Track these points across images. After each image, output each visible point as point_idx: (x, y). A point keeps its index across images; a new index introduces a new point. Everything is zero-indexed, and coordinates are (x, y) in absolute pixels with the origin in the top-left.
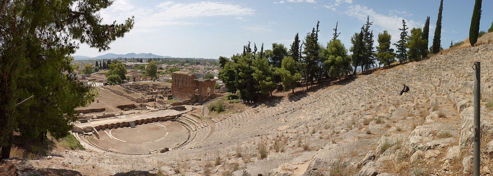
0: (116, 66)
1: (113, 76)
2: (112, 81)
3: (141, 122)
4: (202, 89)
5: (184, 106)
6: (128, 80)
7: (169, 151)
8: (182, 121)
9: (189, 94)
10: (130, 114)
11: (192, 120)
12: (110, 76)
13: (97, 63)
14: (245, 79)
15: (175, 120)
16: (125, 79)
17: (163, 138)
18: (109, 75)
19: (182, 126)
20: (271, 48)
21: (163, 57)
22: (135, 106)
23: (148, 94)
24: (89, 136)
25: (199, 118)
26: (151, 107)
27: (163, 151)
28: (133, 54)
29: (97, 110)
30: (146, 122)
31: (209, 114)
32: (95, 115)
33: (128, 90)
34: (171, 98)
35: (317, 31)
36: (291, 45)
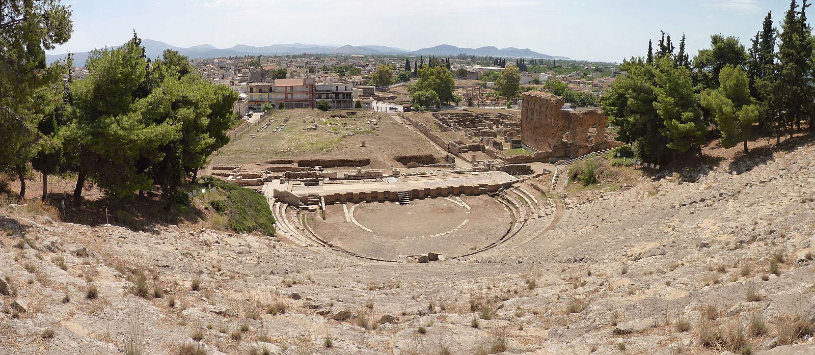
0: (432, 74)
1: (424, 93)
2: (424, 103)
3: (423, 194)
4: (578, 130)
5: (528, 164)
6: (457, 103)
7: (437, 262)
8: (509, 198)
9: (550, 139)
11: (529, 197)
12: (418, 92)
13: (408, 63)
14: (642, 114)
15: (498, 195)
16: (453, 100)
17: (449, 232)
18: (415, 90)
19: (506, 209)
20: (708, 46)
21: (552, 57)
22: (434, 159)
23: (476, 135)
24: (308, 212)
25: (543, 193)
26: (469, 162)
27: (423, 260)
29: (349, 161)
30: (434, 193)
31: (566, 188)
32: (341, 172)
33: (443, 125)
34: (518, 145)
35: (805, 6)
36: (752, 39)
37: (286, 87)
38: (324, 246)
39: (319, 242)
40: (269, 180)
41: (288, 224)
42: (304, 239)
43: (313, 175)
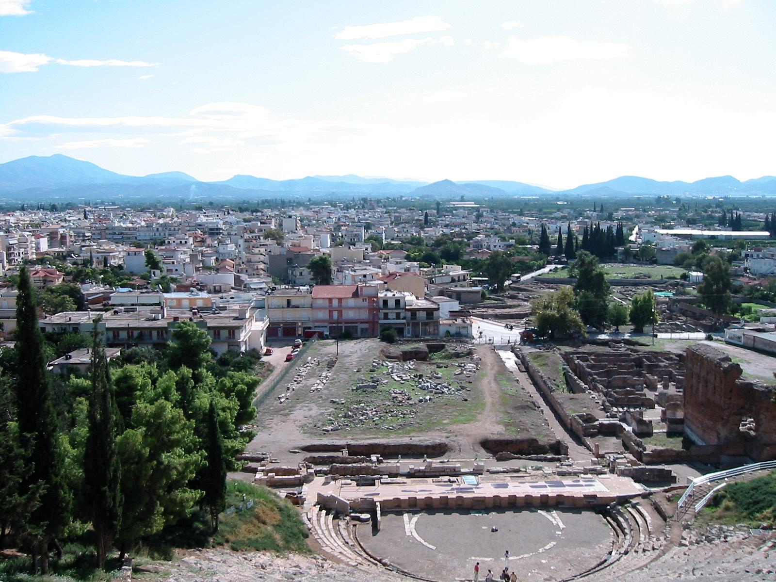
5: (667, 467)
9: (719, 427)
10: (504, 472)
17: (526, 556)
28: (729, 179)
37: (330, 300)
38: (376, 565)
39: (372, 560)
40: (307, 480)
41: (336, 538)
42: (354, 556)
43: (367, 470)
